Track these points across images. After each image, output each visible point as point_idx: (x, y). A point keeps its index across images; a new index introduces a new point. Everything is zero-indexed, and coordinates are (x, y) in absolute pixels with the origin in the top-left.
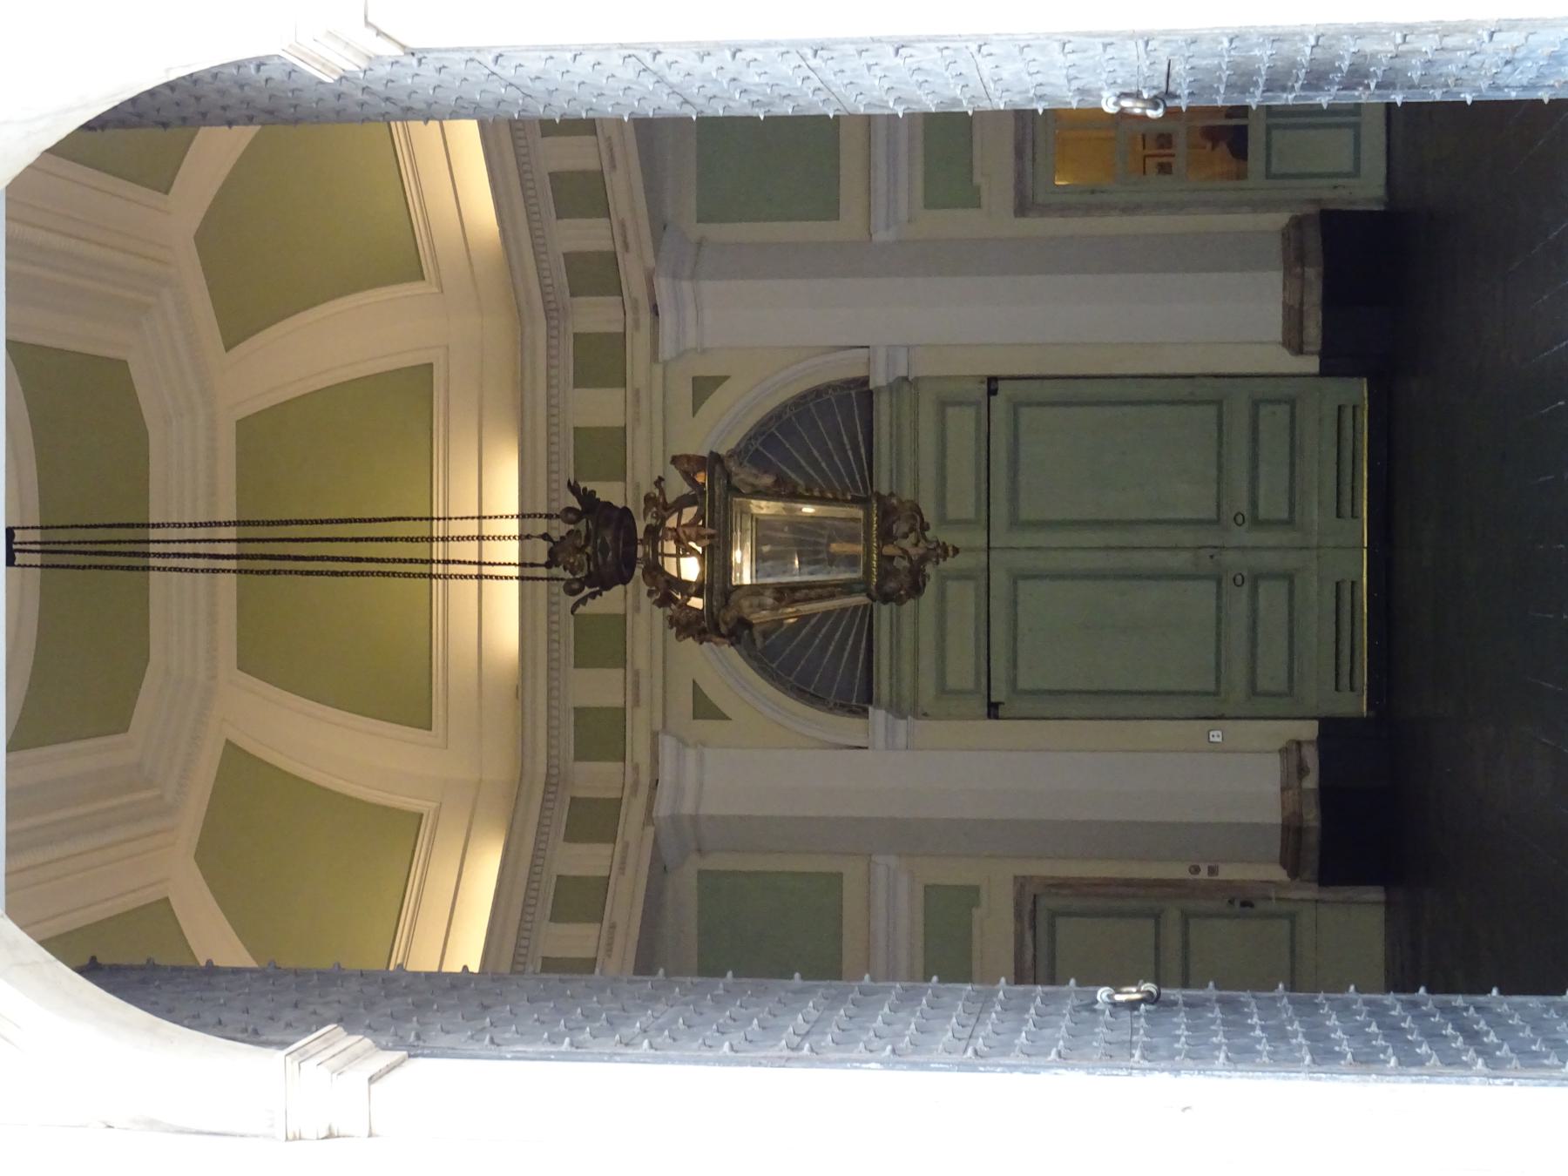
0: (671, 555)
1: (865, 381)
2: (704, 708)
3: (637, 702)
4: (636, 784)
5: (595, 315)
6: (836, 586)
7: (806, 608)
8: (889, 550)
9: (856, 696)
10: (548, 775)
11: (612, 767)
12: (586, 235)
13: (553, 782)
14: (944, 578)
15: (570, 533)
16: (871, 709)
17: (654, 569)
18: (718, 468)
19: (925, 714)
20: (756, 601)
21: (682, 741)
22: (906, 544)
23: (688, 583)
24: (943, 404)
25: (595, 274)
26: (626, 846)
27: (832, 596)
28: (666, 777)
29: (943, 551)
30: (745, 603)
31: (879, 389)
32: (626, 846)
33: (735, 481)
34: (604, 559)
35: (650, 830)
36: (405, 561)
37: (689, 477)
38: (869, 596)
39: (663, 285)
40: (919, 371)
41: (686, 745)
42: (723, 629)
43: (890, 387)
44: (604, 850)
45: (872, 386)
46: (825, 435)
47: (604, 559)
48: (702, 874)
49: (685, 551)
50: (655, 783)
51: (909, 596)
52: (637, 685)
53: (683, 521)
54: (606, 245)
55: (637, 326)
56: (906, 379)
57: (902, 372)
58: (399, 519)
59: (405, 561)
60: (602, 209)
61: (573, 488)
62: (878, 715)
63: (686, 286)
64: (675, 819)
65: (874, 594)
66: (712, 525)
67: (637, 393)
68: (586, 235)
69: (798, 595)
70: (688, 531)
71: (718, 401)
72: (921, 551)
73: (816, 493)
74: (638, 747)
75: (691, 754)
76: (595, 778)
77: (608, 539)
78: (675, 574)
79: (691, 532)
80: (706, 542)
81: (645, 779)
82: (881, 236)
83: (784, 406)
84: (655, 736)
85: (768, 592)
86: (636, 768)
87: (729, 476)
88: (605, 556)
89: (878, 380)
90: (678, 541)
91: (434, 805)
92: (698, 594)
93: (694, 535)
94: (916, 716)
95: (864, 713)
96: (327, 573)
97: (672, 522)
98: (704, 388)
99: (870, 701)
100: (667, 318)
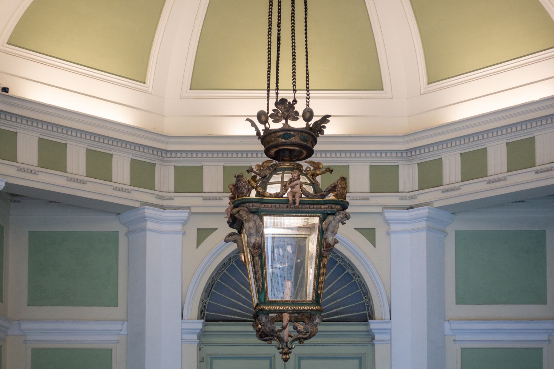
0: (282, 178)
1: (372, 317)
2: (203, 234)
3: (205, 199)
4: (162, 198)
5: (408, 176)
6: (263, 284)
7: (250, 267)
8: (286, 317)
9: (210, 313)
10: (167, 151)
11: (172, 186)
12: (452, 168)
14: (270, 358)
15: (297, 113)
16: (202, 321)
17: (275, 170)
18: (339, 207)
19: (200, 349)
20: (253, 231)
21: (185, 223)
22: (290, 328)
23: (265, 188)
24: (360, 358)
25: (430, 175)
26: (129, 191)
27: (256, 280)
28: (168, 214)
29: (286, 353)
30: (251, 224)
31: (368, 325)
32: (129, 191)
33: (331, 218)
34: (279, 137)
35: (137, 205)
36: (279, 13)
37: (333, 189)
38: (257, 305)
39: (424, 211)
40: (378, 347)
41: (184, 225)
42: (235, 210)
43: (370, 331)
44: (127, 179)
45: (370, 321)
46: (343, 296)
47: (279, 137)
48: (116, 234)
49: (284, 186)
50: (163, 208)
51: (258, 331)
52: (215, 198)
53: (304, 186)
54: (446, 180)
55: (402, 198)
56: (373, 338)
57: (377, 337)
58: (306, 8)
59: (279, 13)
60: (466, 177)
61: (325, 119)
62: (199, 325)
63: (423, 224)
64: (144, 219)
65: (259, 307)
67: (367, 199)
68: (452, 168)
69: (257, 259)
71: (362, 241)
72: (286, 338)
73: (322, 271)
74: (182, 200)
75: (179, 227)
76: (165, 176)
77: (293, 139)
79: (297, 189)
80: (291, 199)
81: (165, 203)
82: (447, 325)
83: (360, 276)
84: (189, 208)
85: (259, 239)
86: (171, 198)
87: (333, 214)
88: (283, 137)
89: (373, 325)
90: (291, 181)
91: (150, 91)
92: (258, 194)
93: (294, 190)
95: (202, 315)
96: (270, 24)
97: (303, 179)
98: (369, 234)
99: (207, 321)
100: (406, 214)
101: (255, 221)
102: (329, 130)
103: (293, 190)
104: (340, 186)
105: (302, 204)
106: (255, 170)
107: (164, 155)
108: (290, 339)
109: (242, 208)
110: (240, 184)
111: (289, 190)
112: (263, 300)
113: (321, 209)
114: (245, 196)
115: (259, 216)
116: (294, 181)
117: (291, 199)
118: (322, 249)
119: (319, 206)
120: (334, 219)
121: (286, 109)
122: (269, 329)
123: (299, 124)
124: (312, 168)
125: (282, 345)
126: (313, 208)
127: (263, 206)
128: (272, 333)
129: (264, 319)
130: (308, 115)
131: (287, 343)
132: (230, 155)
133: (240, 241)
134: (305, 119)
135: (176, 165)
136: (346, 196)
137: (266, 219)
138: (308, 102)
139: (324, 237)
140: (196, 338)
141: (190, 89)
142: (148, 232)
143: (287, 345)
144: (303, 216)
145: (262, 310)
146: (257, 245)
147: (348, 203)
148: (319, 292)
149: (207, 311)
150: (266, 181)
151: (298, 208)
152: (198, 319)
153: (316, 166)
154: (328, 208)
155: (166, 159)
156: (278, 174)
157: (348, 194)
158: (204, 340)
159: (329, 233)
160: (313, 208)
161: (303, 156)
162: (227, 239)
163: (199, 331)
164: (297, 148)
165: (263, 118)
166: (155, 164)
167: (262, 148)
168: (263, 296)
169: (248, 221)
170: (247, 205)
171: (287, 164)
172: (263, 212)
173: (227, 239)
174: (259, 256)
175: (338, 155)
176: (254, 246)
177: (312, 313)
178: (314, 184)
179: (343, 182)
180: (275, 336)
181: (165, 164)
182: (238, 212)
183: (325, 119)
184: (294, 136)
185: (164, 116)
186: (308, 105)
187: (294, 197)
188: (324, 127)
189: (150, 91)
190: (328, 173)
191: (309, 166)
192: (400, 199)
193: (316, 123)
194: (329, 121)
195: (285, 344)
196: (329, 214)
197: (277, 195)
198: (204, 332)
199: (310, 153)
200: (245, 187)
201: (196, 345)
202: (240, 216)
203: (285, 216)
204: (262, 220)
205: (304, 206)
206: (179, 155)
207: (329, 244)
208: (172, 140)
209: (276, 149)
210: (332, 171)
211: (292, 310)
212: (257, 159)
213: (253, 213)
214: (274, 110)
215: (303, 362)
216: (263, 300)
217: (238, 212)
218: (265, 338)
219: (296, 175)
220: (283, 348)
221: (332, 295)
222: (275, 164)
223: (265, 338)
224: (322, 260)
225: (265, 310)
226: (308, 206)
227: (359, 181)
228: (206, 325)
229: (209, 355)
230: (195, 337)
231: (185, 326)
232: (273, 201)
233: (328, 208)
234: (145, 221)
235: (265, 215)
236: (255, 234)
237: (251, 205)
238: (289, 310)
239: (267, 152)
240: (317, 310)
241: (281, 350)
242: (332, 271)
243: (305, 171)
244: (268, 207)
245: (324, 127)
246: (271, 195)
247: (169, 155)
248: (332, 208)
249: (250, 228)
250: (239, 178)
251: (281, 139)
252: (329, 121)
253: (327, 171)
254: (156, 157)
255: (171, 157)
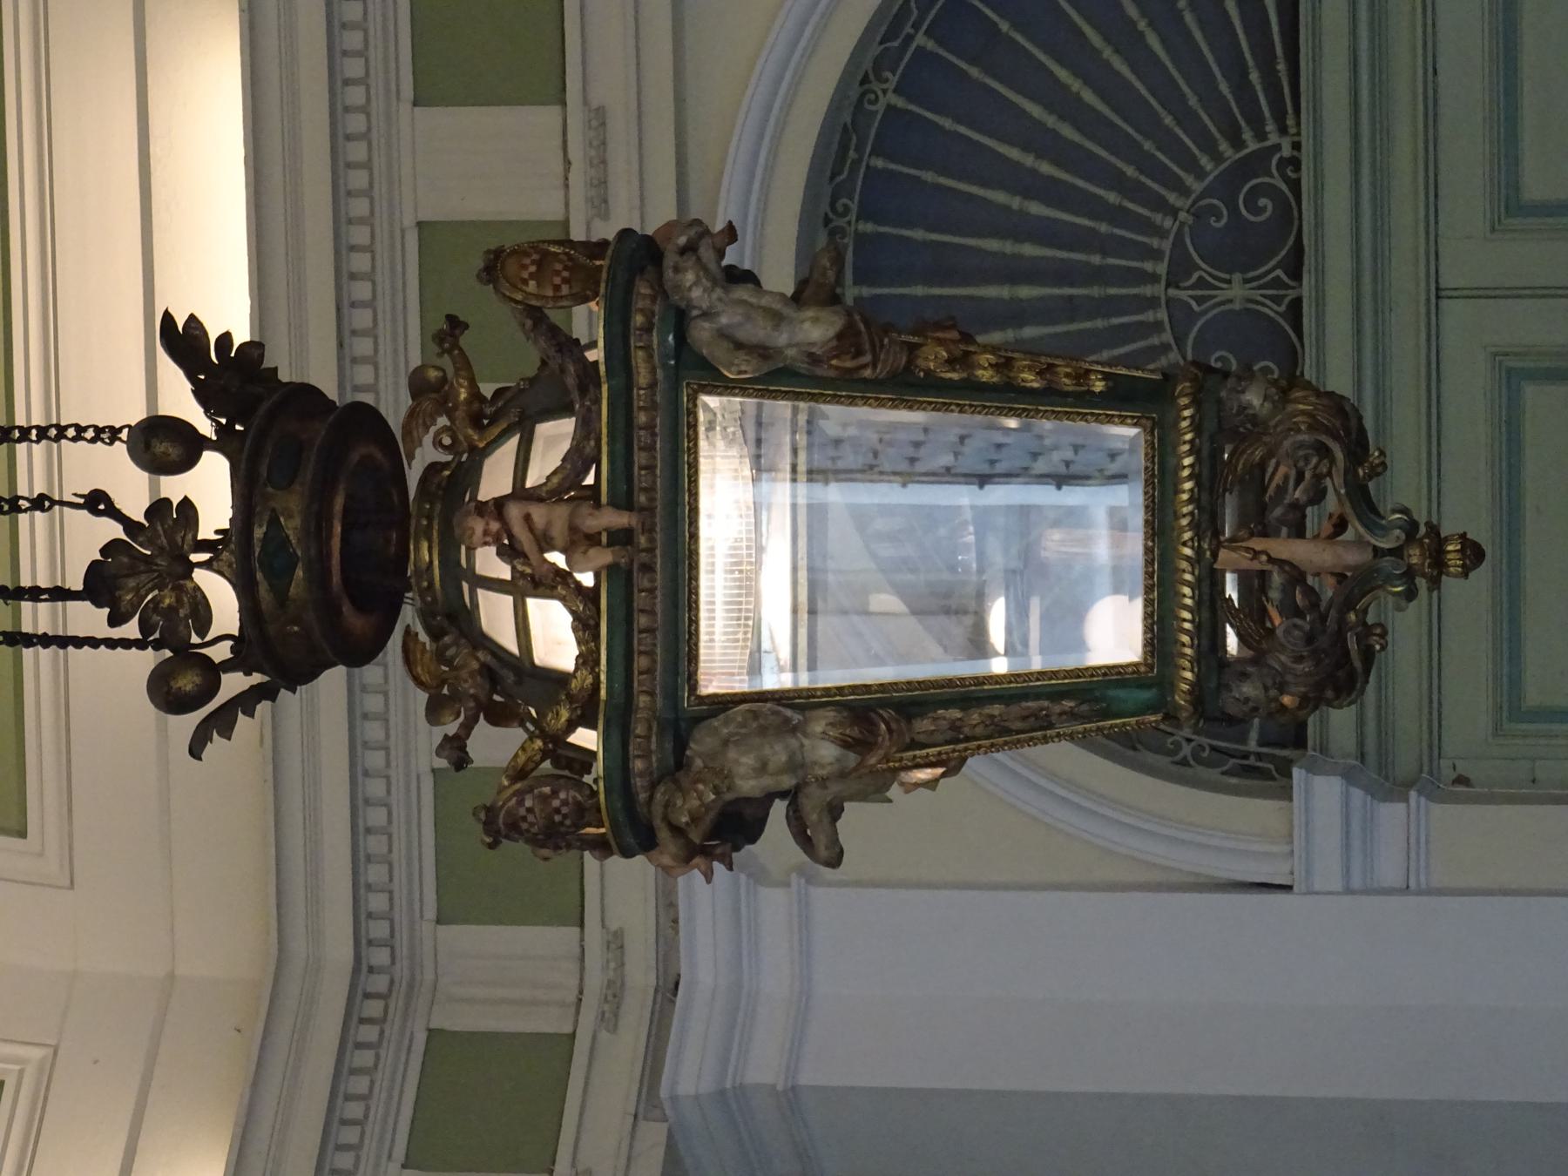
4: (615, 993)
6: (1057, 695)
10: (359, 966)
13: (371, 993)
15: (159, 507)
16: (1297, 773)
17: (456, 620)
19: (1462, 780)
23: (555, 680)
29: (1431, 555)
33: (702, 333)
35: (654, 1135)
49: (534, 583)
50: (669, 988)
53: (533, 479)
62: (1321, 793)
64: (731, 1101)
66: (623, 501)
69: (923, 725)
70: (539, 513)
73: (985, 375)
77: (292, 527)
78: (510, 643)
80: (605, 557)
81: (641, 976)
86: (616, 943)
87: (681, 319)
88: (280, 577)
90: (510, 552)
94: (1434, 793)
101: (726, 743)
102: (229, 314)
103: (559, 541)
104: (532, 286)
105: (630, 493)
106: (452, 728)
107: (379, 983)
108: (1355, 529)
109: (658, 810)
110: (535, 822)
111: (557, 558)
112: (1146, 695)
113: (652, 386)
114: (594, 794)
115: (698, 720)
116: (511, 537)
117: (605, 557)
118: (867, 373)
119: (640, 396)
120: (706, 315)
121: (141, 572)
122: (1299, 659)
123: (210, 489)
124: (443, 421)
125: (1390, 579)
126: (650, 427)
127: (643, 700)
128: (1323, 642)
129: (1248, 689)
130: (163, 444)
131: (1378, 552)
132: (376, 817)
133: (835, 788)
134: (187, 461)
135: (431, 912)
136: (586, 245)
137: (719, 672)
138: (99, 431)
139: (803, 367)
140: (1400, 807)
141: (23, 834)
142: (806, 1078)
143: (1391, 552)
144: (694, 451)
145: (1198, 694)
146: (855, 732)
147: (626, 234)
148: (1099, 386)
149: (1243, 739)
150: (512, 684)
151: (650, 510)
152: (1290, 799)
153: (427, 405)
154: (647, 348)
155: (402, 970)
156: (475, 605)
157: (578, 235)
158: (1405, 759)
159: (782, 339)
160: (650, 427)
161: (379, 455)
162: (823, 852)
163: (1357, 794)
164: (339, 503)
165: (187, 682)
166: (431, 1032)
167: (334, 678)
168: (1121, 693)
169: (723, 777)
170: (639, 783)
171: (425, 553)
172: (673, 696)
173: (823, 852)
174: (909, 719)
175: (358, 179)
176: (859, 745)
177: (1210, 425)
178: (518, 414)
179: (511, 267)
180: (1342, 621)
181: (429, 976)
182: (677, 830)
183: (183, 341)
184: (274, 522)
185: (171, 976)
186: (114, 433)
187: (592, 540)
188: (225, 339)
189: (36, 1053)
190: (465, 341)
191: (428, 439)
192: (614, 1029)
193: (203, 395)
194: (192, 318)
195: (1386, 563)
196: (681, 338)
197: (585, 627)
198: (1362, 756)
199: (364, 419)
200: (544, 799)
201: (1437, 809)
202: (695, 819)
203: (694, 537)
204: (723, 704)
205: (640, 477)
206: (376, 873)
207: (840, 336)
208: (299, 946)
209: (347, 608)
210: (452, 320)
211: (1199, 536)
212: (395, 719)
213: (681, 745)
214: (114, 621)
215: (1535, 188)
216: (1146, 695)
217: (677, 830)
218: (1358, 664)
219: (478, 525)
220: (1409, 575)
221: (1142, 25)
222: (426, 615)
223: (1358, 664)
224: (928, 372)
225: (1197, 686)
226: (640, 458)
227: (498, 168)
228: (1323, 749)
229: (1497, 730)
230: (1392, 814)
231: (1328, 873)
232: (619, 650)
233: (647, 348)
234: (741, 1090)
235: (694, 686)
236: (794, 743)
237: (638, 765)
238: (1199, 551)
239: (360, 653)
240: (1196, 402)
241: (1422, 583)
242: (1004, 26)
243: (458, 454)
244: (650, 671)
245: (225, 339)
246: (587, 659)
247: (380, 957)
248: (648, 329)
249: (762, 768)
250: (498, 827)
251: (293, 591)
252: (192, 318)
253: (455, 345)
254: (392, 1030)
255: (389, 944)
